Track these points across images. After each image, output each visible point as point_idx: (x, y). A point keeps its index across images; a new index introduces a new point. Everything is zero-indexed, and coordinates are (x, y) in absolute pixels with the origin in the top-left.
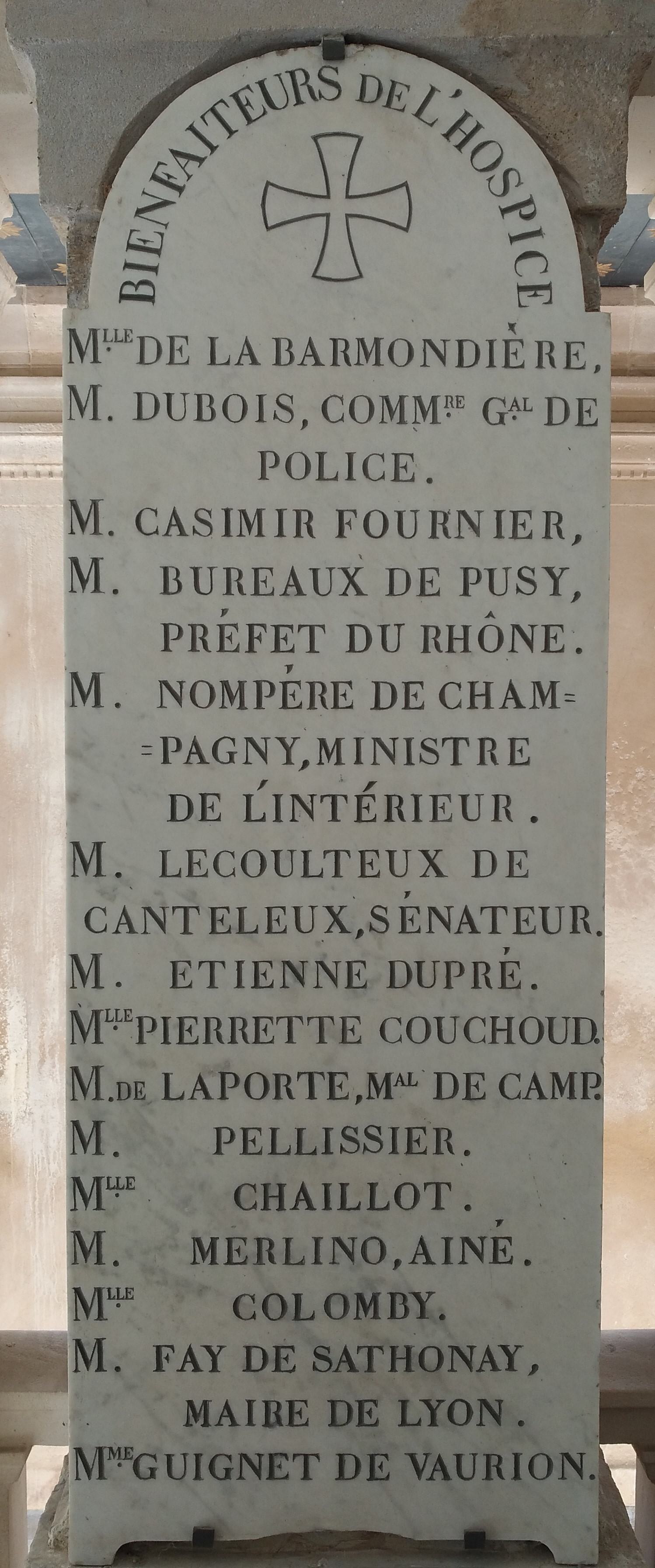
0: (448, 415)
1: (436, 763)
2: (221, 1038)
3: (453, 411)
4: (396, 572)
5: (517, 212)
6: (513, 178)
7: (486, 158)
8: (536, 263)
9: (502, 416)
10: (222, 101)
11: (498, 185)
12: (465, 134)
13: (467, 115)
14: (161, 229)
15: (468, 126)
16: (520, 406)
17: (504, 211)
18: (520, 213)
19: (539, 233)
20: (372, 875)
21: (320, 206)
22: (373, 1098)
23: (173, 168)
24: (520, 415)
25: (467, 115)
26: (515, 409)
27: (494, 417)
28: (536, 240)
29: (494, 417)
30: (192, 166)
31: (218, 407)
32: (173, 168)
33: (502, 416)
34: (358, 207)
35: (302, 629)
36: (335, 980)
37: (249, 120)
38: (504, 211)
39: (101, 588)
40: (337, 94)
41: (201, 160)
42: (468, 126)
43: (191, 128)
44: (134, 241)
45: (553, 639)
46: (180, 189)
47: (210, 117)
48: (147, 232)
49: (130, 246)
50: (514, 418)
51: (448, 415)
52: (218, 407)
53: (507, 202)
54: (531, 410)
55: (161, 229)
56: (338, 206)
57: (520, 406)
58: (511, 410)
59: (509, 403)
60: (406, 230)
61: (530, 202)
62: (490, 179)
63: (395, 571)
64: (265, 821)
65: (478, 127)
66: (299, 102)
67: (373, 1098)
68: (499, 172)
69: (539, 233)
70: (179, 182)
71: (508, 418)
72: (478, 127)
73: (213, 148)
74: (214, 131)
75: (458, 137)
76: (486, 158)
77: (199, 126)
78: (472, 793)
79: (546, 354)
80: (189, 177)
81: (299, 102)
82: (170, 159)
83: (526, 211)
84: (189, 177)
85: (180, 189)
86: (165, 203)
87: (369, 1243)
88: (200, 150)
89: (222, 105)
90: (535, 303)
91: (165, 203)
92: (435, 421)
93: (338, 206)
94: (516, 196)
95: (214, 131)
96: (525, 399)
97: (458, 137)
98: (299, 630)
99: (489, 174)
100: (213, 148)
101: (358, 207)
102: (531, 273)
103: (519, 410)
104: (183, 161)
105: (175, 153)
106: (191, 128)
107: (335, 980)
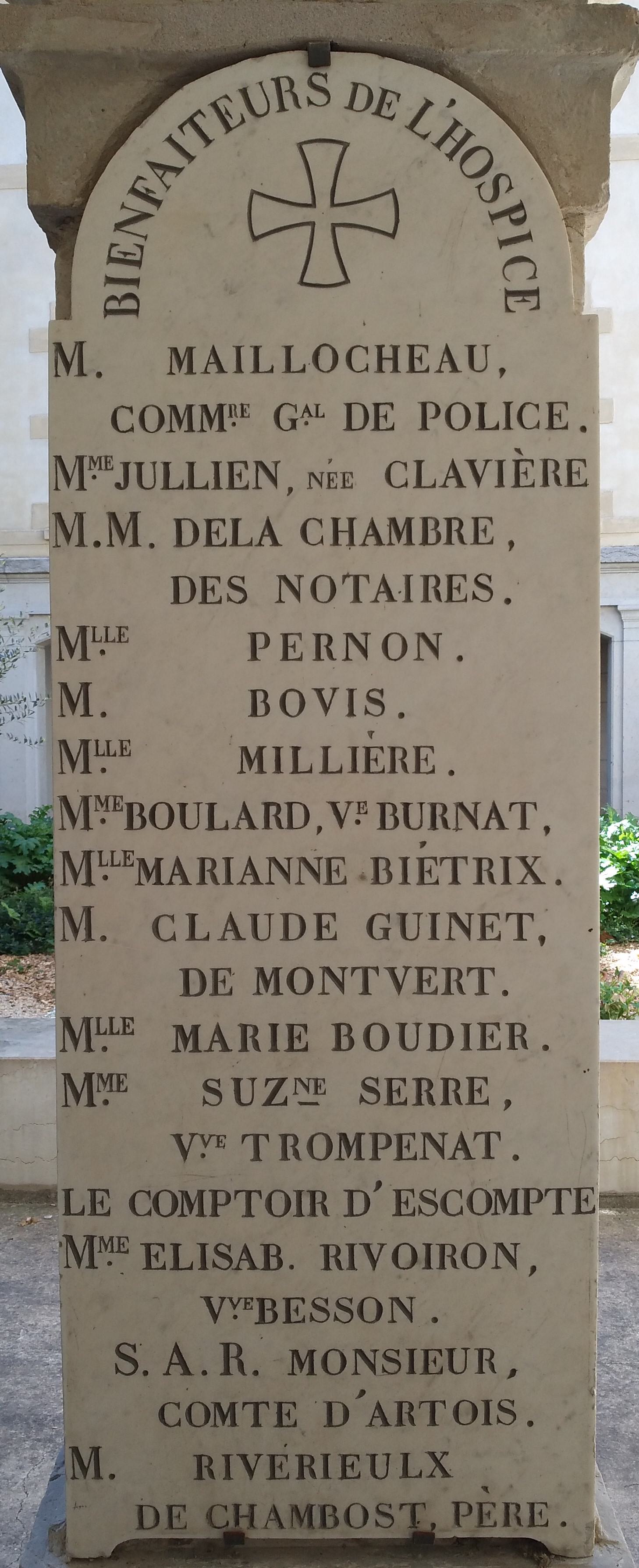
0: (234, 424)
1: (219, 1103)
3: (238, 420)
4: (438, 1028)
6: (503, 184)
8: (525, 269)
9: (294, 422)
10: (200, 112)
11: (488, 192)
12: (456, 141)
13: (457, 124)
14: (141, 241)
16: (313, 412)
17: (494, 217)
19: (529, 236)
21: (323, 201)
24: (313, 421)
25: (457, 124)
26: (306, 415)
27: (286, 424)
28: (526, 244)
29: (286, 424)
31: (340, 1514)
33: (294, 422)
35: (79, 1210)
36: (321, 484)
37: (228, 129)
38: (494, 217)
42: (459, 134)
43: (170, 139)
44: (115, 254)
45: (423, 761)
48: (126, 243)
49: (111, 260)
50: (306, 423)
51: (234, 424)
52: (340, 1514)
53: (497, 207)
54: (323, 416)
55: (141, 241)
57: (313, 412)
58: (303, 417)
59: (301, 409)
60: (393, 235)
61: (520, 207)
62: (479, 187)
63: (294, 804)
66: (282, 109)
68: (489, 177)
71: (300, 423)
72: (469, 134)
75: (449, 145)
78: (245, 1075)
81: (282, 109)
82: (147, 172)
83: (519, 215)
85: (158, 203)
86: (147, 216)
88: (177, 160)
92: (221, 428)
93: (323, 215)
94: (506, 201)
95: (190, 140)
96: (317, 406)
97: (449, 145)
103: (311, 415)
107: (321, 484)
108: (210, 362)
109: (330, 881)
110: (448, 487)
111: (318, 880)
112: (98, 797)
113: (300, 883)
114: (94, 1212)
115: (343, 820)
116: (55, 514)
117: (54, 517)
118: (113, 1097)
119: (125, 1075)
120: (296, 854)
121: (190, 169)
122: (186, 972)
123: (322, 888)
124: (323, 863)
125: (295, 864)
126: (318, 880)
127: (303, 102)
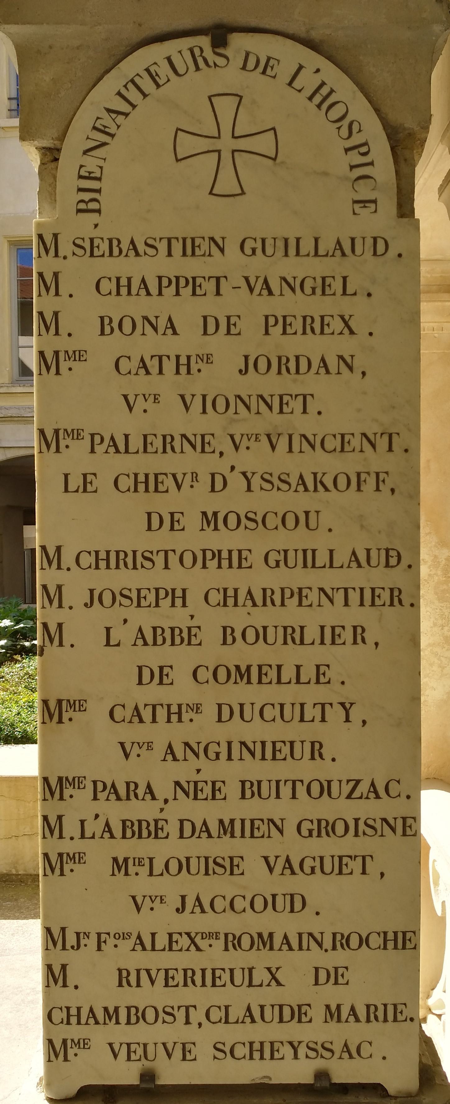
2: (127, 565)
5: (356, 151)
6: (355, 127)
7: (336, 113)
10: (138, 75)
11: (344, 132)
14: (101, 163)
15: (325, 91)
17: (347, 150)
18: (359, 152)
19: (372, 164)
20: (279, 1058)
21: (226, 156)
22: (261, 950)
23: (107, 120)
25: (323, 84)
30: (120, 119)
32: (107, 120)
34: (242, 144)
35: (162, 240)
37: (158, 86)
39: (60, 332)
40: (226, 63)
41: (126, 115)
42: (325, 91)
43: (119, 94)
44: (83, 173)
46: (113, 136)
47: (130, 86)
48: (91, 164)
53: (349, 144)
56: (226, 143)
62: (339, 128)
64: (102, 167)
65: (332, 91)
67: (261, 950)
68: (346, 123)
69: (372, 164)
70: (112, 131)
72: (332, 91)
73: (134, 106)
74: (133, 95)
75: (318, 99)
76: (336, 113)
77: (124, 92)
79: (132, 791)
80: (118, 127)
82: (105, 115)
84: (118, 127)
85: (113, 136)
86: (104, 144)
87: (248, 947)
88: (125, 107)
89: (137, 77)
90: (364, 213)
91: (104, 144)
93: (226, 143)
94: (356, 139)
95: (133, 95)
97: (318, 99)
98: (160, 241)
99: (338, 125)
100: (134, 106)
101: (242, 144)
102: (364, 192)
104: (114, 116)
105: (109, 111)
106: (119, 94)
108: (141, 287)
109: (196, 798)
110: (320, 374)
111: (188, 797)
112: (68, 701)
113: (258, 413)
114: (85, 490)
115: (248, 593)
116: (48, 1040)
117: (47, 1041)
118: (76, 867)
119: (84, 853)
120: (254, 393)
121: (134, 114)
122: (149, 514)
123: (190, 802)
124: (192, 785)
125: (254, 399)
126: (188, 797)
127: (211, 63)
